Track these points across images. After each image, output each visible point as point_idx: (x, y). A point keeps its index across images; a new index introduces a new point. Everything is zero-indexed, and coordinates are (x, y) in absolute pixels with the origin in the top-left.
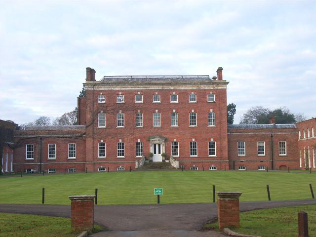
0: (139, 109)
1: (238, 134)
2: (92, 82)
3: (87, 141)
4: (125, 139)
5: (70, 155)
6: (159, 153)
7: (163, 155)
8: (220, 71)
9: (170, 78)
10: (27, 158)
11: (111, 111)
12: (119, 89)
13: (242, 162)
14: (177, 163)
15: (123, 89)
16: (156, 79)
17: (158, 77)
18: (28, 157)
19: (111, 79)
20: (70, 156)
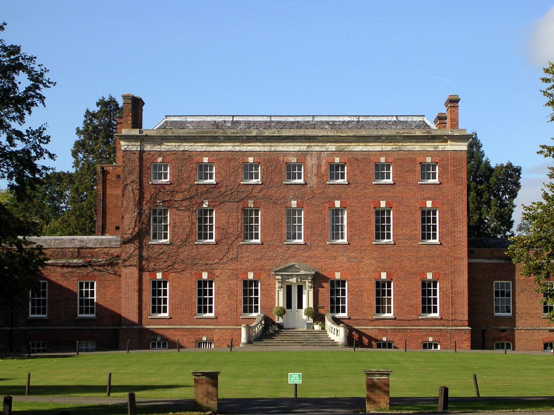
0: (249, 198)
1: (495, 261)
2: (136, 132)
3: (390, 392)
4: (217, 273)
5: (81, 309)
6: (300, 306)
7: (308, 313)
8: (179, 351)
9: (328, 123)
10: (31, 316)
11: (186, 203)
12: (204, 149)
13: (504, 330)
14: (342, 330)
15: (211, 149)
16: (293, 123)
17: (299, 119)
18: (33, 313)
19: (182, 125)
20: (81, 312)
